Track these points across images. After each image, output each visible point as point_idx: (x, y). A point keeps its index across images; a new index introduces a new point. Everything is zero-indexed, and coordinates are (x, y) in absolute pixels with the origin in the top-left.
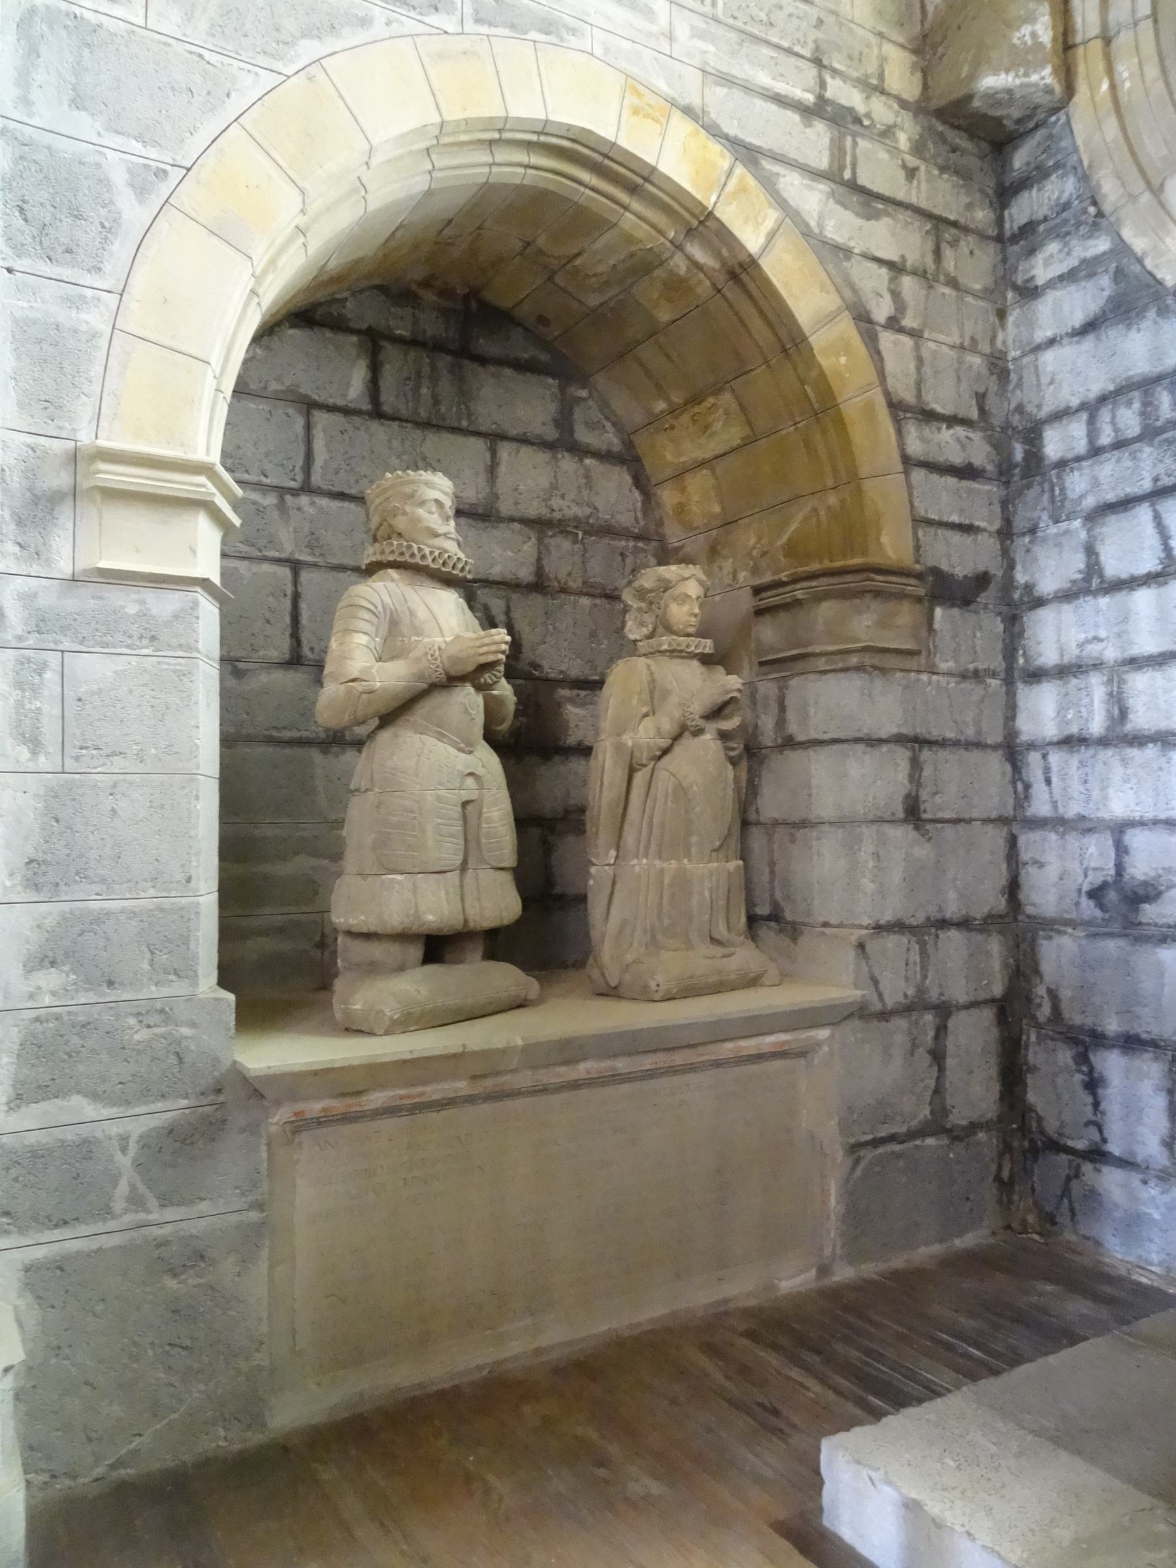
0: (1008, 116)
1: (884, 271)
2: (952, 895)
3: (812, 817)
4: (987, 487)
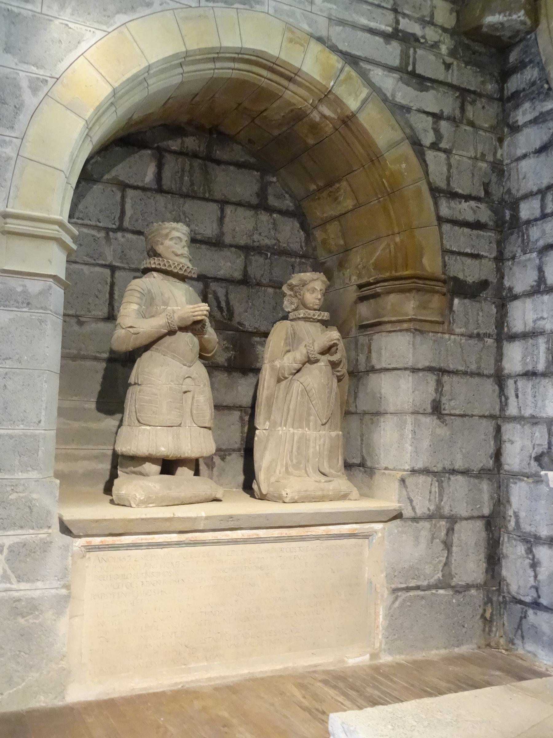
0: (503, 35)
1: (430, 119)
2: (459, 456)
3: (382, 410)
4: (489, 234)
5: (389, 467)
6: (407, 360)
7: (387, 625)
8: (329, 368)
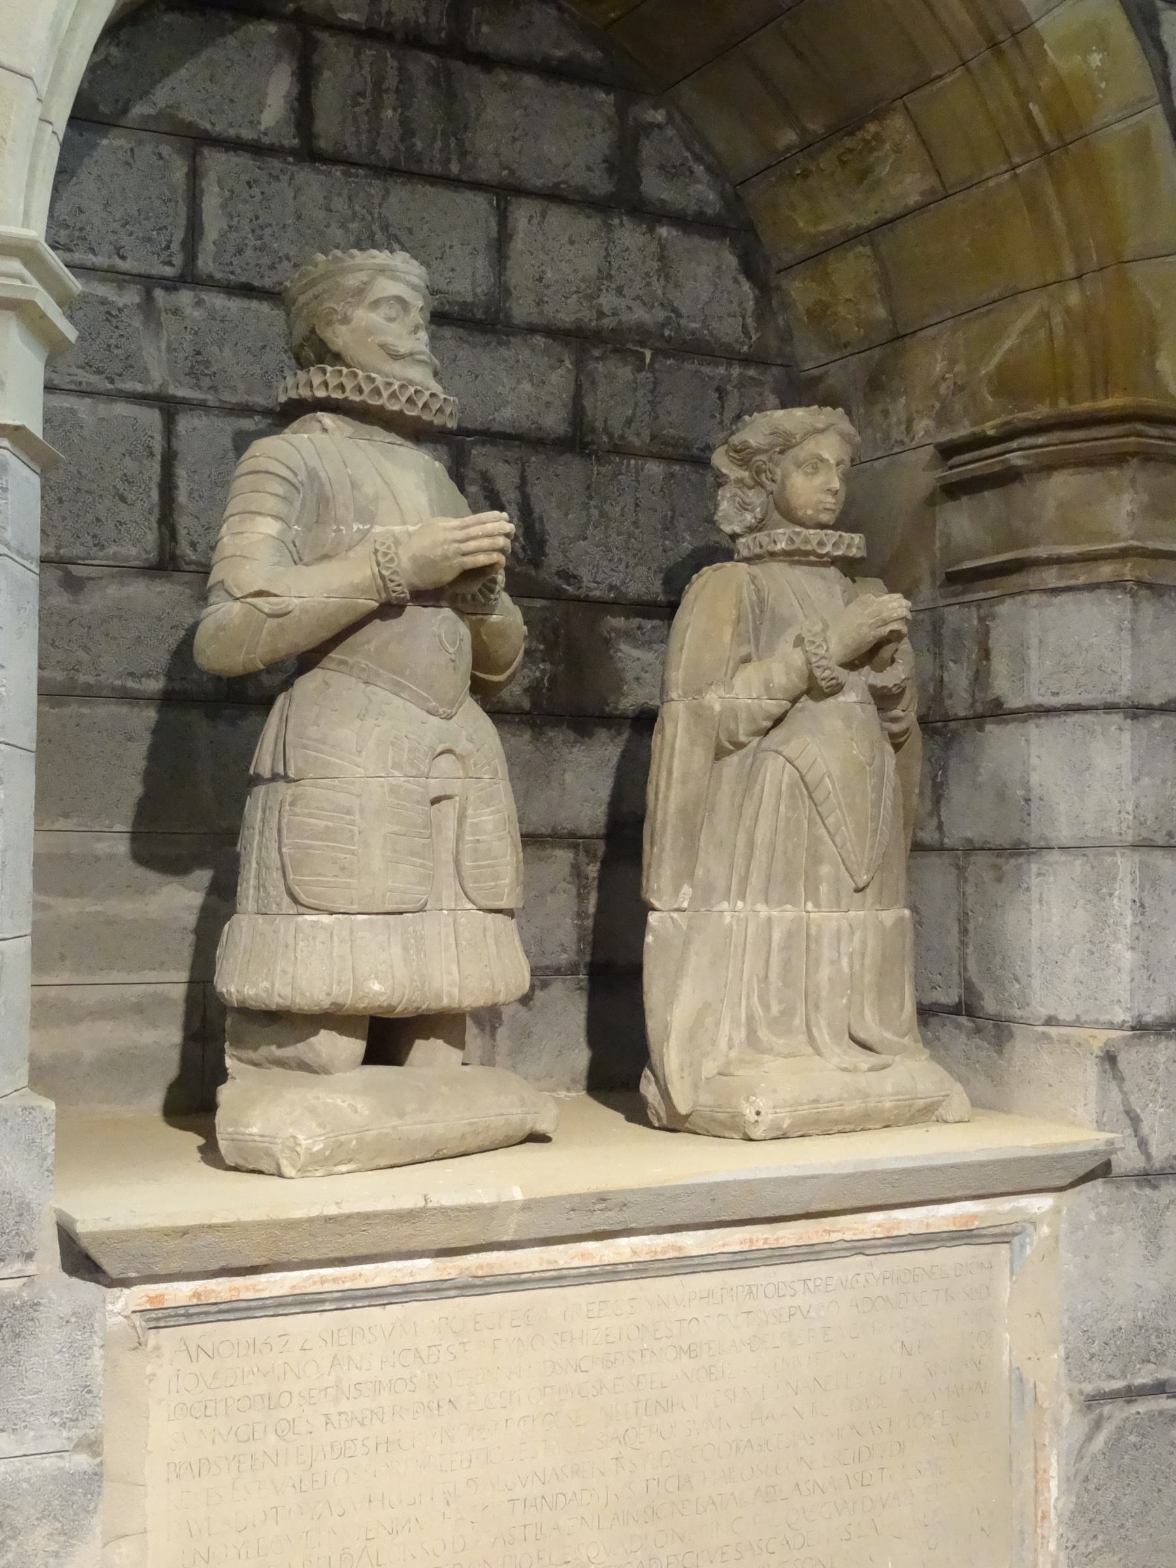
3: (1032, 837)
5: (1061, 1017)
6: (1115, 678)
7: (1072, 1507)
8: (872, 708)
